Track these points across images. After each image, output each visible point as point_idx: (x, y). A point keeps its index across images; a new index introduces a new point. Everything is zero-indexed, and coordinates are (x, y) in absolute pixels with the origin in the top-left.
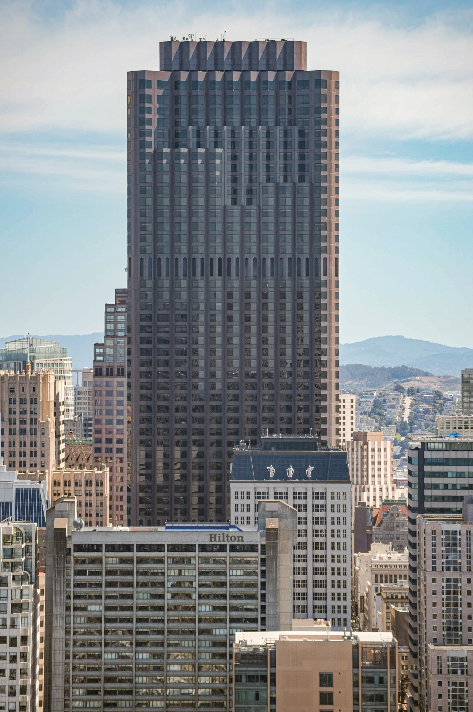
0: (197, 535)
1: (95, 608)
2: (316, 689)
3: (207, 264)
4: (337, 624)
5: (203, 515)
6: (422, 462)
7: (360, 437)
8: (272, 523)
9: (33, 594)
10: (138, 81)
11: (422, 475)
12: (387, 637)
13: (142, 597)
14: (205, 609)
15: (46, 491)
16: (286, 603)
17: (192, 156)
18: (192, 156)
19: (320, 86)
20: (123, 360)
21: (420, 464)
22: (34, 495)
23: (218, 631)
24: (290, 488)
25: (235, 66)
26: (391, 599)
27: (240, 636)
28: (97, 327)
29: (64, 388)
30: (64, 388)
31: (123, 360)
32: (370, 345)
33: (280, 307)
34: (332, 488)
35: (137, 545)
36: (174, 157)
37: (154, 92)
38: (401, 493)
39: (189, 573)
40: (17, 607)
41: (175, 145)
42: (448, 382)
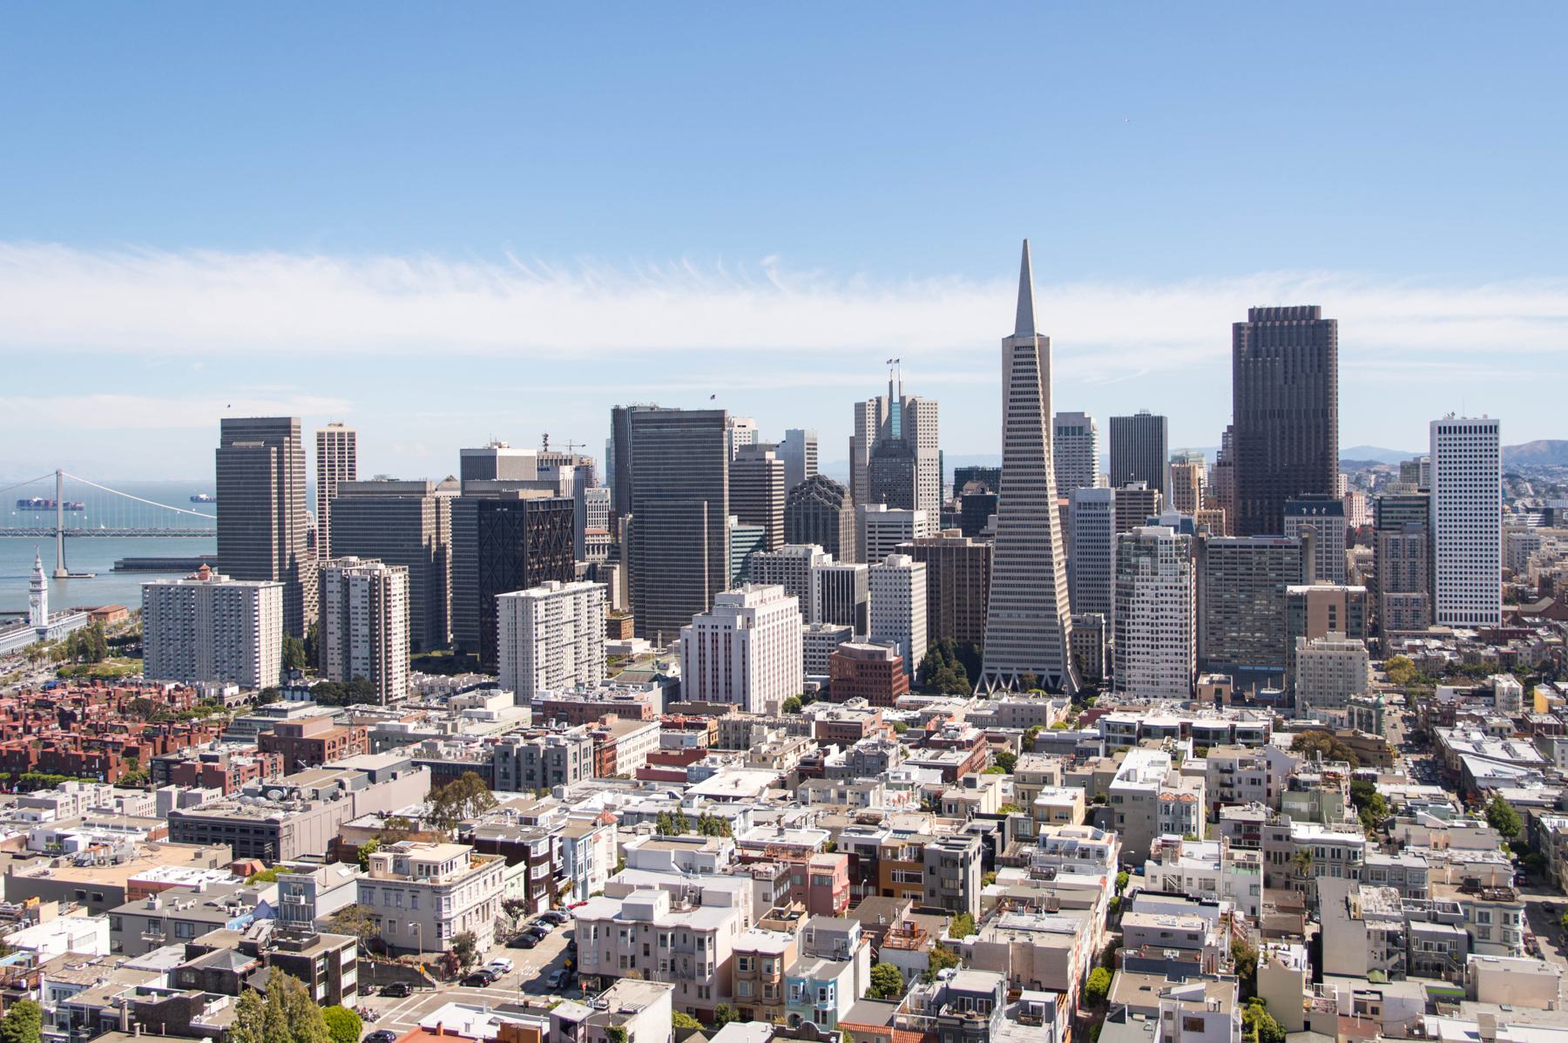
0: (1268, 540)
1: (1219, 574)
2: (1327, 613)
3: (1272, 414)
4: (1338, 583)
5: (1271, 532)
6: (1380, 506)
7: (1349, 494)
8: (1305, 536)
9: (1191, 567)
10: (1238, 328)
11: (1380, 512)
12: (1362, 589)
13: (1242, 569)
14: (1273, 575)
15: (1195, 521)
16: (1312, 573)
17: (1264, 362)
18: (1264, 362)
19: (1328, 327)
20: (1231, 459)
21: (1379, 507)
22: (1189, 522)
23: (1279, 586)
24: (1314, 519)
25: (1286, 318)
26: (1364, 571)
27: (1289, 588)
28: (1218, 444)
29: (1202, 474)
30: (1202, 474)
31: (1231, 459)
32: (1353, 450)
33: (1309, 432)
34: (1334, 519)
35: (1117, 425)
36: (1256, 362)
37: (1246, 332)
38: (1370, 521)
39: (1264, 559)
40: (1182, 573)
41: (1256, 356)
42: (1393, 468)
